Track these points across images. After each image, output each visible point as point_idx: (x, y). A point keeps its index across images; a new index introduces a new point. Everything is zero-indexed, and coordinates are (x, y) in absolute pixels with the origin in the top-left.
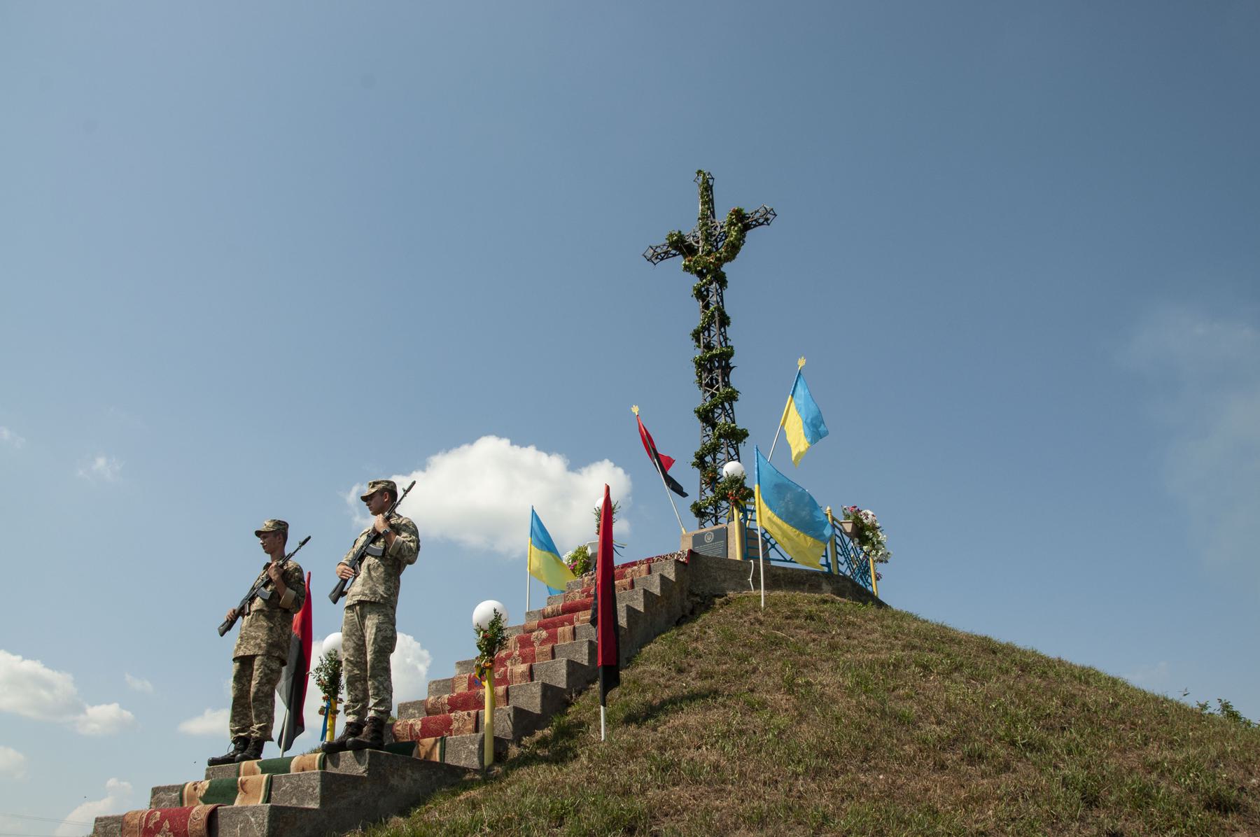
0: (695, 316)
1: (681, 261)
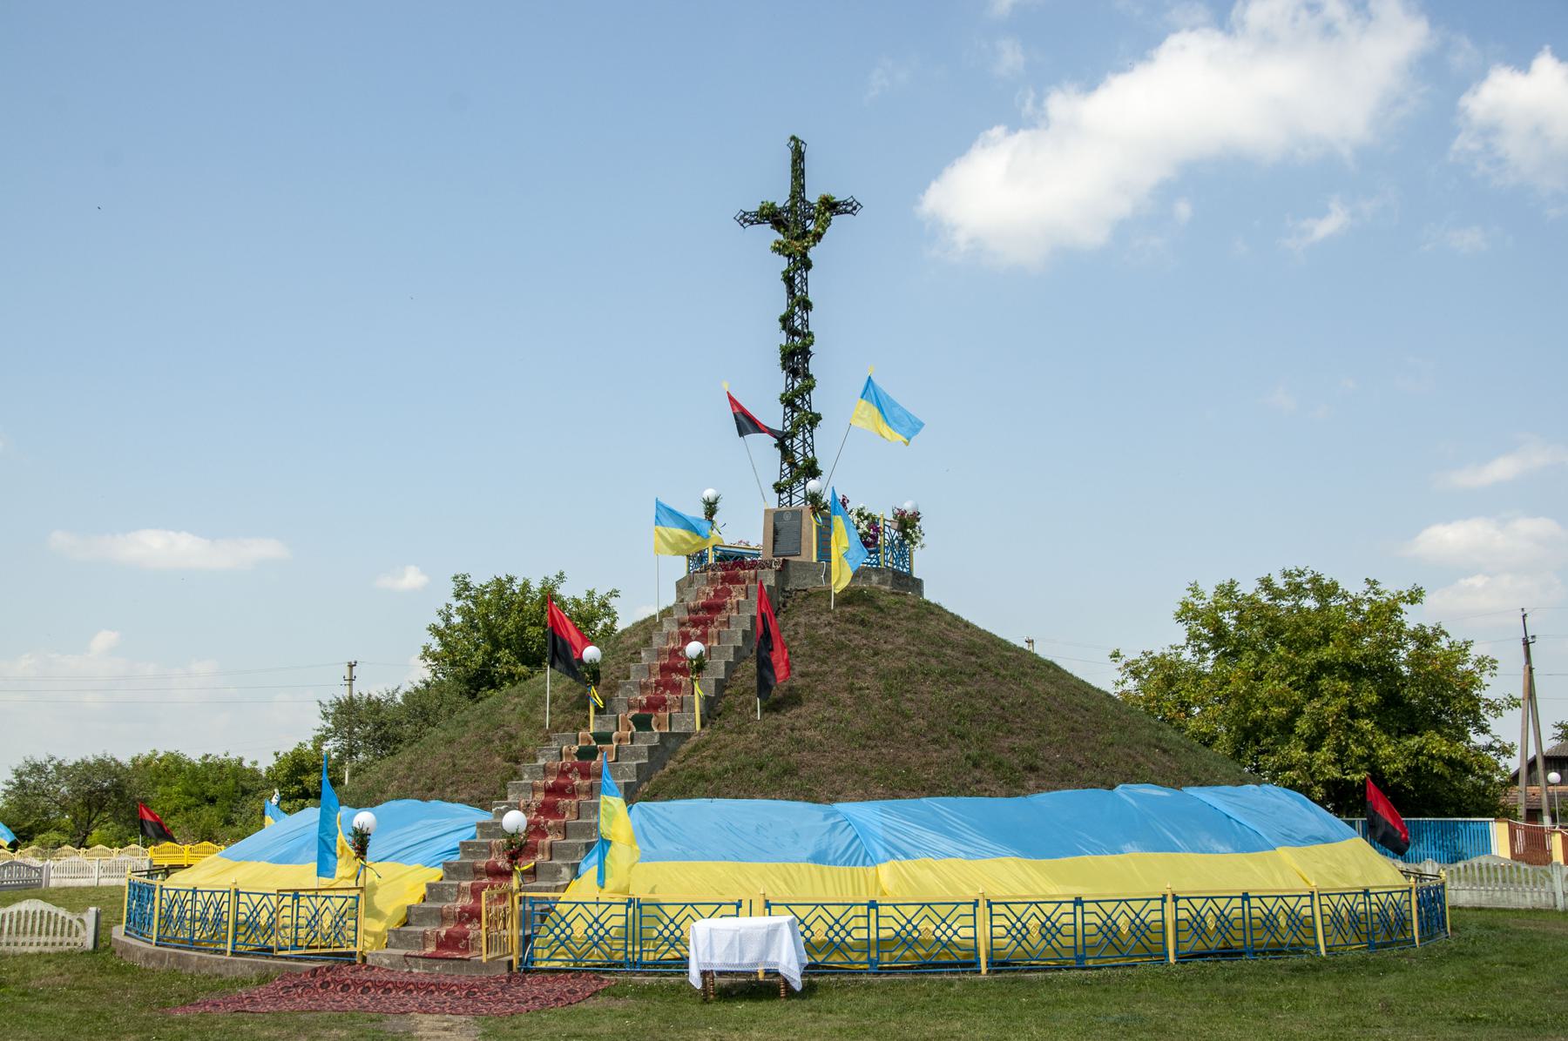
0: (781, 304)
1: (774, 236)
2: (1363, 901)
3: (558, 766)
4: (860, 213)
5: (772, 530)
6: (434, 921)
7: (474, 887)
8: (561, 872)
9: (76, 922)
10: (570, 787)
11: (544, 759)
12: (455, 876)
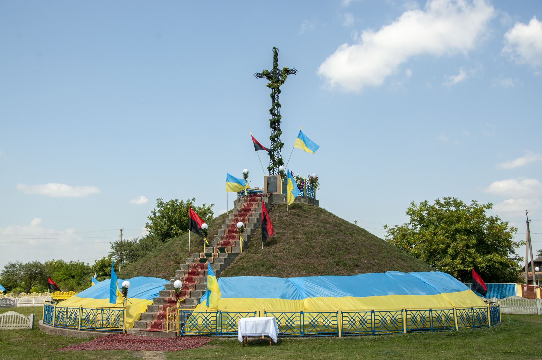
0: (270, 105)
1: (267, 82)
2: (471, 311)
3: (193, 265)
4: (297, 74)
5: (267, 183)
6: (150, 319)
7: (164, 307)
8: (194, 301)
9: (26, 319)
10: (197, 272)
11: (188, 263)
12: (157, 303)
